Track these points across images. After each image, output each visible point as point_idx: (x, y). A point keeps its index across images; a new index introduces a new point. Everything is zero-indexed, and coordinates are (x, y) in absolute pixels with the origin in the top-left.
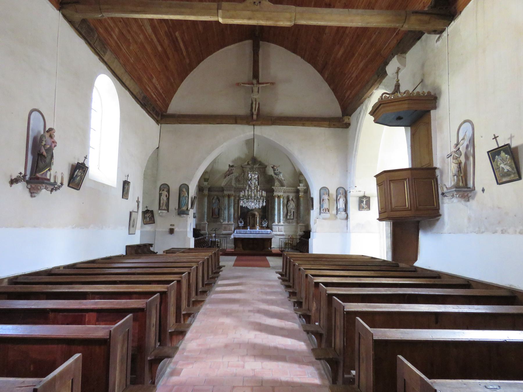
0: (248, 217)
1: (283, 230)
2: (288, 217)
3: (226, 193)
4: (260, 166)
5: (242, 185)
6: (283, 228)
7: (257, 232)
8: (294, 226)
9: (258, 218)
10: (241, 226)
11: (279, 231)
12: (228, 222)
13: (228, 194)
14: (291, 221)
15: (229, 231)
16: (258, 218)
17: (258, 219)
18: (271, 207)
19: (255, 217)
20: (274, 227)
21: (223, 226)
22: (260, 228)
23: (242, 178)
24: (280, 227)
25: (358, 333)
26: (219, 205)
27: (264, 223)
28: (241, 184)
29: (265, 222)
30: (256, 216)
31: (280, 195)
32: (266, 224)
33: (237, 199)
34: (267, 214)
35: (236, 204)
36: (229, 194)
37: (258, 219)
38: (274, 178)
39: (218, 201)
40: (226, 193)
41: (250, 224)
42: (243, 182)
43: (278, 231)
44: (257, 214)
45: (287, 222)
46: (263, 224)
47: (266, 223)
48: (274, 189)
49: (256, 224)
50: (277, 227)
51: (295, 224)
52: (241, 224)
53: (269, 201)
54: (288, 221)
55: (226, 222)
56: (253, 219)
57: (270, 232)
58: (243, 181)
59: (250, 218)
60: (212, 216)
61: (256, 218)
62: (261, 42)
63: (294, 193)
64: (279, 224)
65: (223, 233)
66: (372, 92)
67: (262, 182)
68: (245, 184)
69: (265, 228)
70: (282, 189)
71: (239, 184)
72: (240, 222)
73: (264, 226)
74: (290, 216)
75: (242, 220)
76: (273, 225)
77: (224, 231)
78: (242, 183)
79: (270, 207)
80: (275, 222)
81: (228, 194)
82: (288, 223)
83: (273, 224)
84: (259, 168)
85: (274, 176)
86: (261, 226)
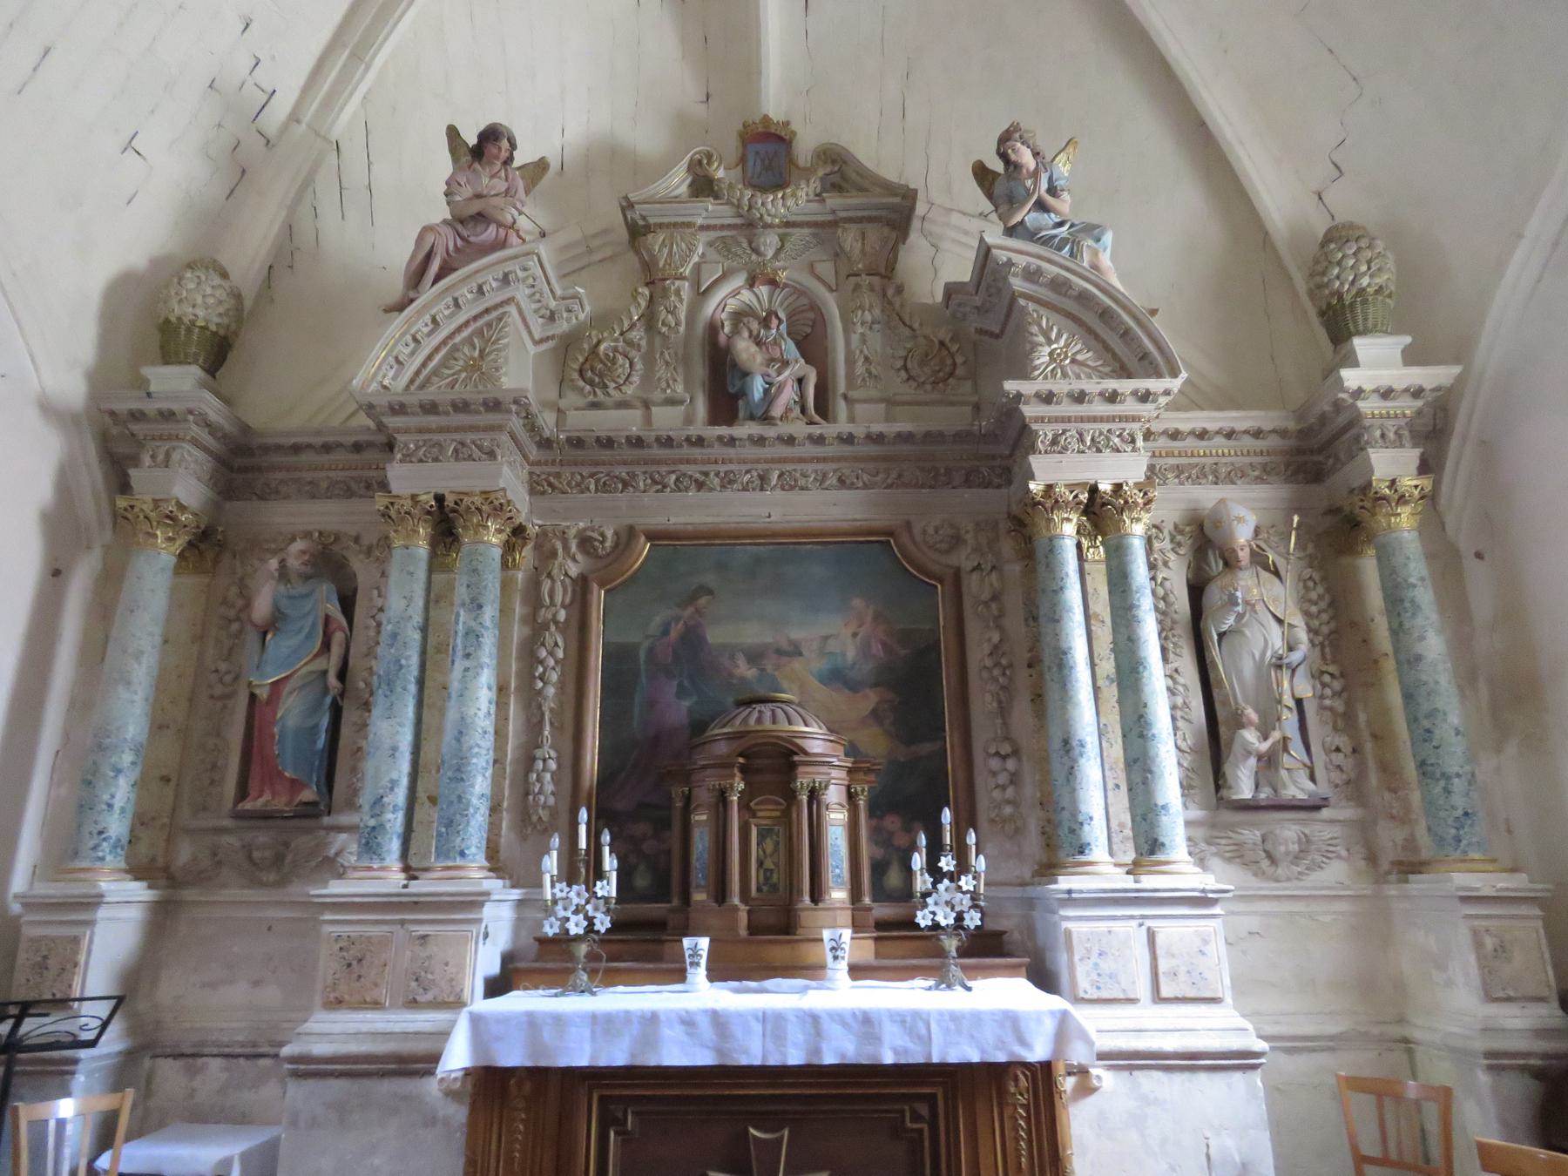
0: (703, 795)
1: (1219, 972)
2: (1244, 785)
3: (408, 479)
4: (834, 201)
5: (637, 414)
6: (1218, 950)
7: (834, 1030)
8: (1344, 906)
9: (834, 795)
10: (576, 927)
11: (1158, 998)
12: (410, 872)
13: (440, 499)
14: (1288, 831)
15: (413, 1004)
16: (834, 795)
17: (836, 821)
18: (995, 650)
19: (791, 796)
20: (1079, 927)
21: (334, 927)
22: (867, 951)
23: (637, 335)
24: (1176, 931)
25: (230, 199)
26: (336, 650)
27: (936, 873)
28: (623, 405)
29: (947, 863)
30: (803, 779)
31: (1118, 487)
32: (966, 882)
33: (574, 570)
34: (951, 739)
35: (554, 636)
36: (450, 501)
37: (836, 821)
38: (1017, 284)
39: (335, 610)
40: (408, 479)
41: (721, 895)
42: (648, 378)
43: (1143, 989)
44: (816, 747)
45: (1238, 856)
46: (922, 882)
47: (963, 867)
48: (1029, 411)
49: (817, 894)
50: (1126, 930)
51: (1335, 873)
52: (576, 894)
53: (972, 584)
54: (1251, 835)
55: (392, 880)
56: (767, 812)
57: (1049, 1026)
58: (639, 366)
59: (722, 797)
60: (243, 793)
61: (814, 794)
62: (791, 786)
63: (1259, 480)
64: (1149, 882)
65: (319, 1049)
66: (676, 938)
67: (860, 368)
68: (672, 402)
69: (951, 944)
70: (1130, 407)
71: (595, 406)
72: (569, 875)
73: (946, 919)
74: (1269, 762)
75: (594, 837)
76: (1070, 899)
77: (337, 1004)
78: (629, 390)
79: (978, 654)
80: (1082, 849)
81: (440, 499)
82: (1249, 864)
83: (1064, 883)
84: (825, 228)
85: (1021, 261)
86: (884, 911)
